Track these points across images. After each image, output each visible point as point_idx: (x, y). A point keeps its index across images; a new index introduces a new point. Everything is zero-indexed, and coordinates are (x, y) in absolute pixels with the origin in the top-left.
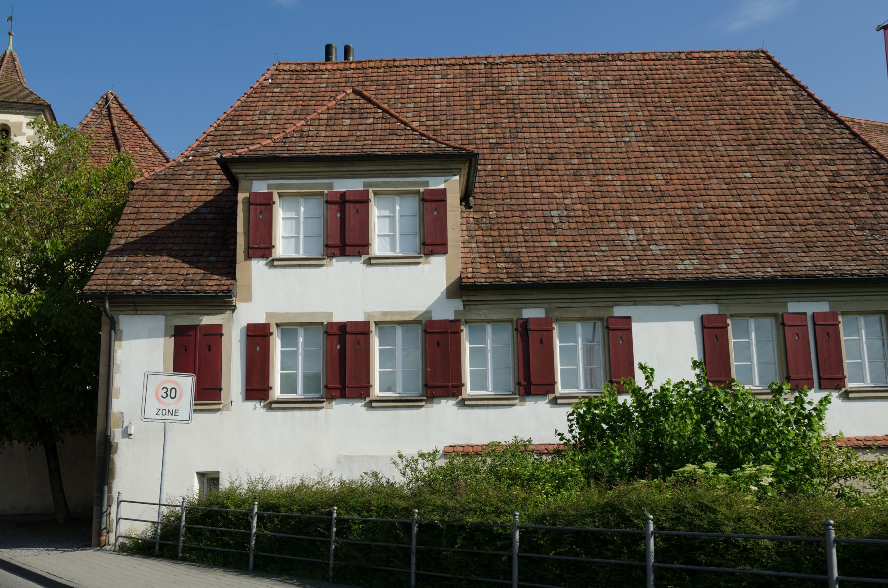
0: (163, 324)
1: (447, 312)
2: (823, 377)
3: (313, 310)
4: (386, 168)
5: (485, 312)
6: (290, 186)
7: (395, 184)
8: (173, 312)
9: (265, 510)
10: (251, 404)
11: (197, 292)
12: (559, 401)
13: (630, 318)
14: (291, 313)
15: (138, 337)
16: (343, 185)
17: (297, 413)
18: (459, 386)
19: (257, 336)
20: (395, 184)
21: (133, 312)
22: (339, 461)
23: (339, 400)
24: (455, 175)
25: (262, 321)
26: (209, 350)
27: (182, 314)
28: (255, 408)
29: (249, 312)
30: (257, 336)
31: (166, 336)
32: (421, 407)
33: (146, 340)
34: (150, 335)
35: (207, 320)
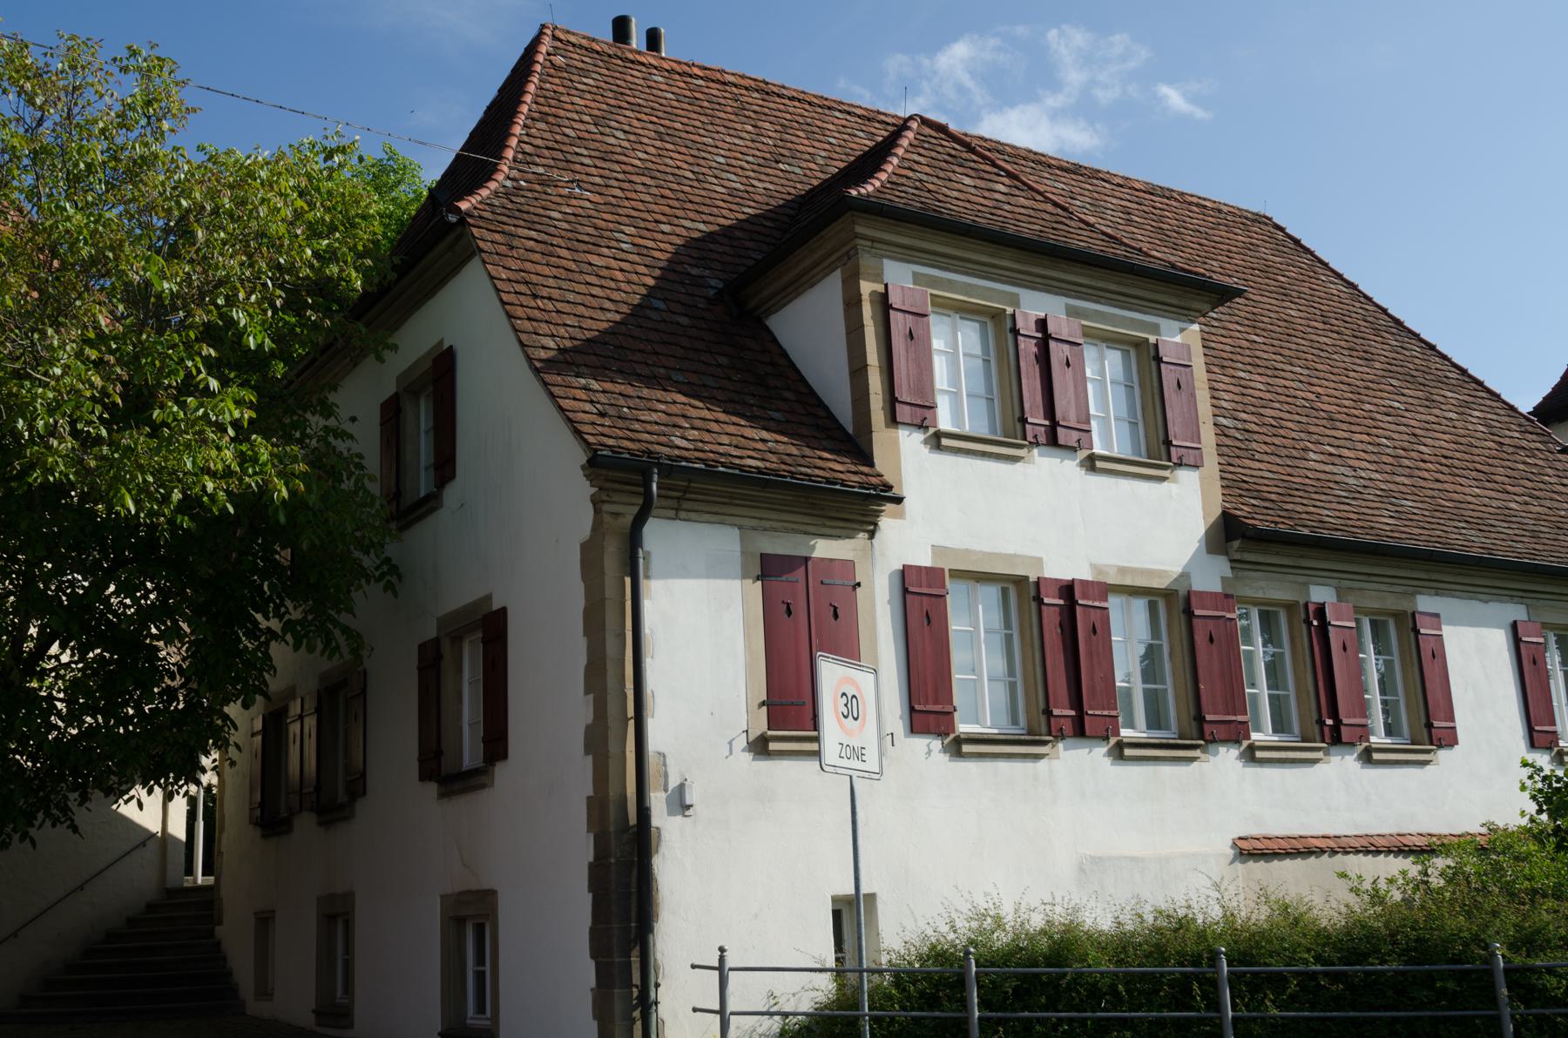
0: (738, 548)
1: (1211, 578)
2: (917, 707)
3: (1009, 549)
4: (1100, 284)
5: (1263, 584)
6: (950, 285)
7: (967, 289)
8: (753, 523)
9: (1242, 963)
10: (921, 743)
11: (828, 481)
12: (773, 746)
13: (1437, 616)
14: (975, 552)
15: (683, 572)
16: (1033, 305)
17: (1002, 765)
18: (1364, 731)
19: (922, 596)
20: (967, 289)
21: (672, 513)
22: (1082, 870)
23: (1069, 741)
24: (1193, 322)
25: (925, 561)
26: (836, 616)
27: (775, 530)
28: (929, 752)
29: (902, 541)
30: (922, 596)
31: (744, 576)
32: (1315, 761)
33: (703, 582)
34: (713, 571)
35: (824, 549)
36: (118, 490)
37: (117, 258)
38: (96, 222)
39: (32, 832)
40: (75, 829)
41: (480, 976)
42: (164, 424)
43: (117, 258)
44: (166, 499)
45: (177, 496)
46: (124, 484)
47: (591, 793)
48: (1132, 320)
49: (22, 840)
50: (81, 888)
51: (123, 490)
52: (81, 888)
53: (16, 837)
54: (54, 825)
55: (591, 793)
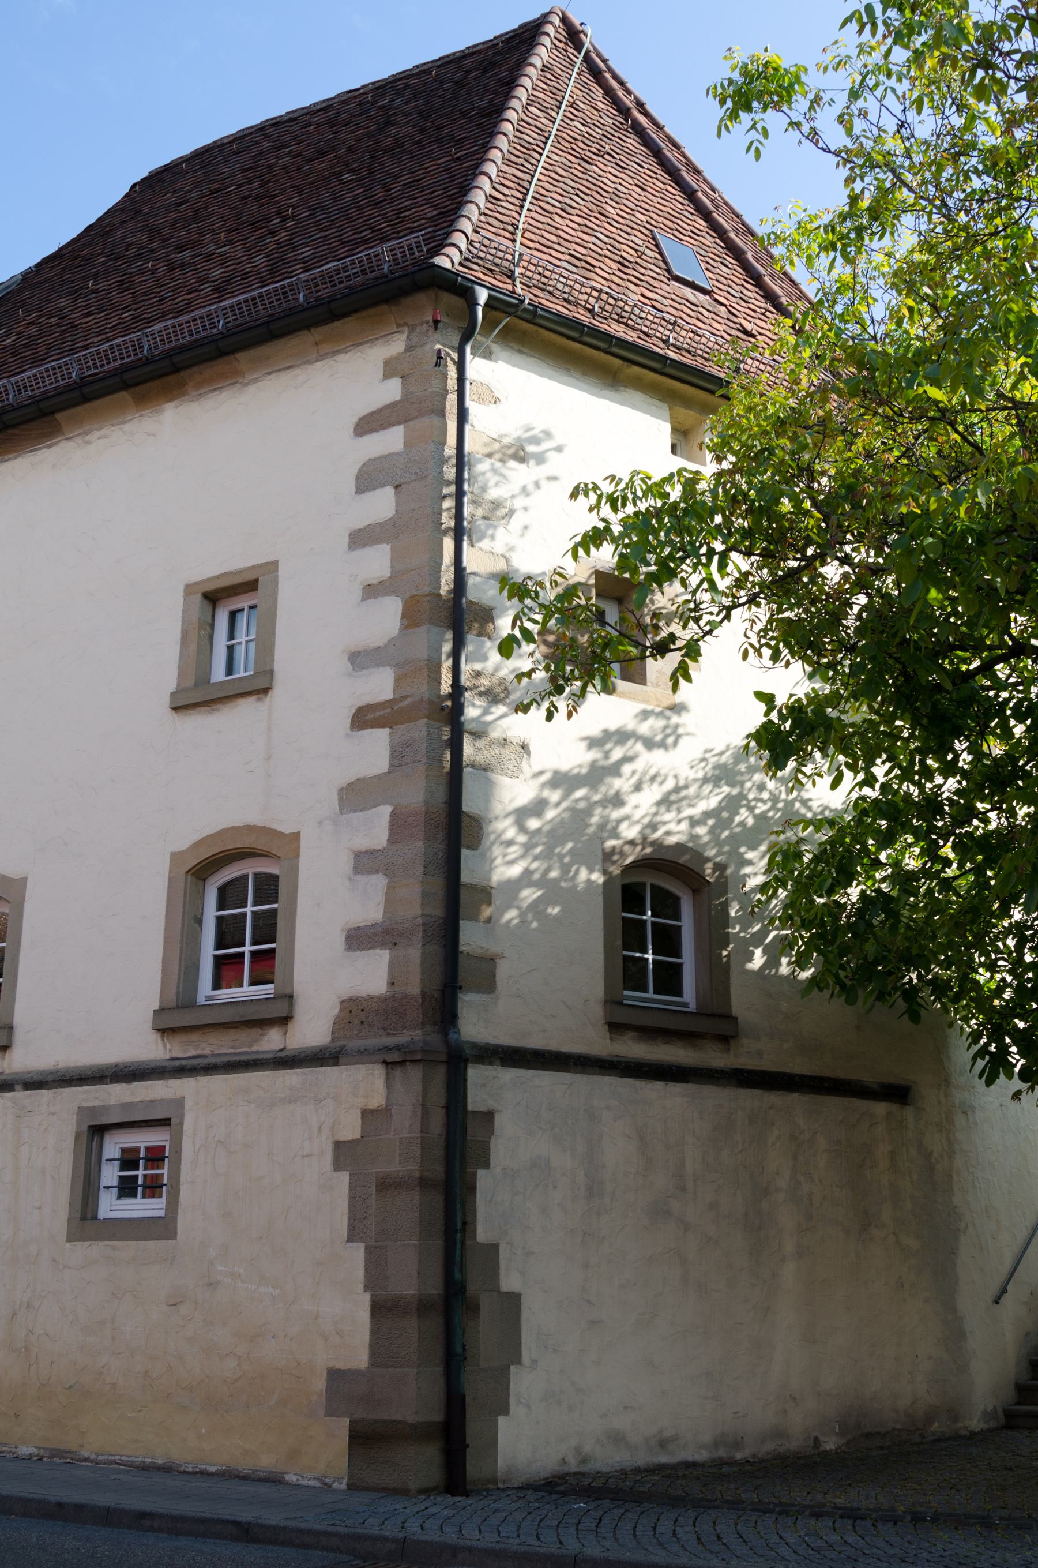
47: (502, 1420)
55: (502, 1420)
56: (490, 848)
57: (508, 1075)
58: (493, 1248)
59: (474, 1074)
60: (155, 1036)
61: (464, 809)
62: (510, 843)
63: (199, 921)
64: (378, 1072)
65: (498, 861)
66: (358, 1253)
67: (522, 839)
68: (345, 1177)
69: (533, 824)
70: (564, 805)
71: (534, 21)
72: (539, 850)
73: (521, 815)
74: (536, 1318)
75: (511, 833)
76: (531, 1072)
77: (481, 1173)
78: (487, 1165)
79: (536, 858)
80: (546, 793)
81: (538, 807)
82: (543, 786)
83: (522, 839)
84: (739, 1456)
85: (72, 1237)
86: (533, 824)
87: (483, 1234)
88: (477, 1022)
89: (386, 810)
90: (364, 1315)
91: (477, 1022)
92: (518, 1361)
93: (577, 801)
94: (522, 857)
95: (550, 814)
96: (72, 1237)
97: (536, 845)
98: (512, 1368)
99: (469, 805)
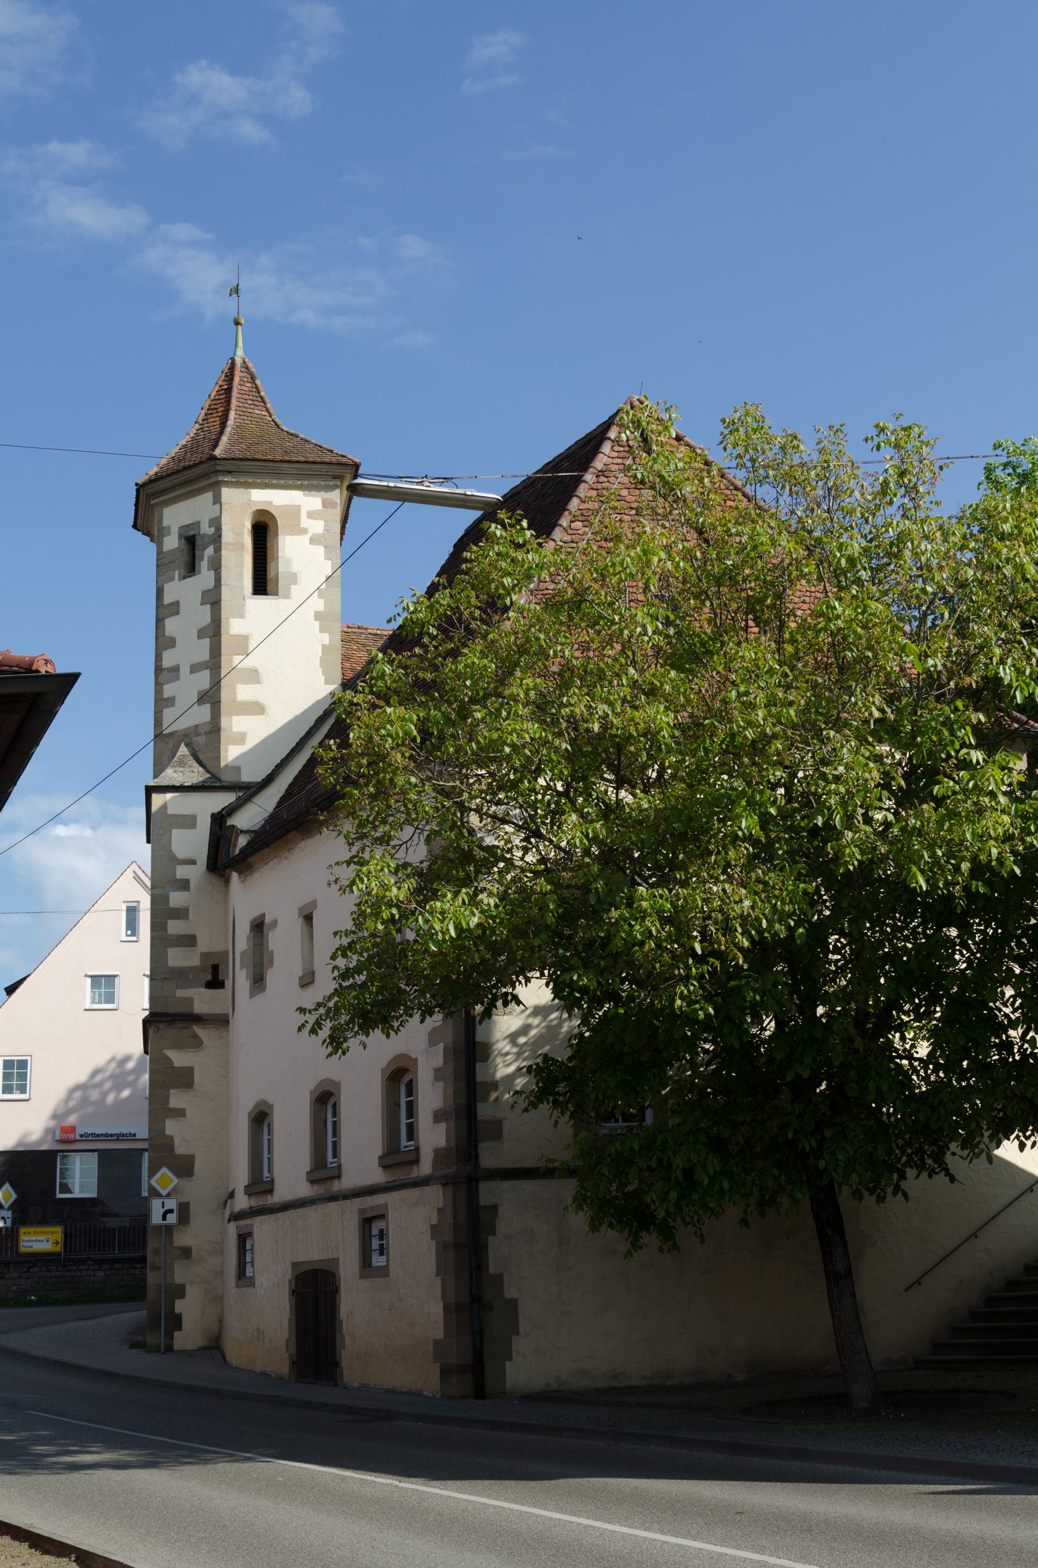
36: (909, 871)
37: (875, 657)
38: (863, 613)
39: (904, 1184)
40: (952, 1179)
41: (219, 1453)
42: (945, 798)
43: (875, 657)
44: (957, 869)
45: (965, 866)
46: (915, 863)
47: (508, 1364)
48: (152, 1440)
49: (895, 1193)
50: (975, 1235)
51: (914, 869)
52: (975, 1235)
53: (890, 1190)
54: (930, 1176)
55: (508, 1364)
56: (494, 1060)
57: (505, 1185)
58: (499, 1278)
59: (483, 1187)
60: (380, 1169)
61: (477, 1039)
62: (507, 1054)
63: (399, 1105)
64: (440, 1188)
65: (500, 1065)
66: (439, 1279)
67: (515, 1050)
68: (434, 1242)
69: (522, 1040)
70: (543, 1025)
71: (604, 423)
72: (526, 1054)
73: (513, 1038)
74: (527, 1311)
75: (508, 1048)
76: (520, 1182)
77: (490, 1238)
78: (494, 1234)
79: (525, 1059)
80: (530, 1021)
81: (525, 1030)
82: (529, 1016)
83: (515, 1050)
84: (669, 1383)
85: (362, 1276)
86: (522, 1040)
87: (492, 1269)
88: (489, 1157)
89: (442, 1045)
90: (441, 1313)
91: (489, 1157)
92: (517, 1333)
93: (552, 1021)
94: (516, 1060)
95: (533, 1032)
96: (362, 1276)
97: (525, 1052)
98: (514, 1337)
99: (479, 1037)
